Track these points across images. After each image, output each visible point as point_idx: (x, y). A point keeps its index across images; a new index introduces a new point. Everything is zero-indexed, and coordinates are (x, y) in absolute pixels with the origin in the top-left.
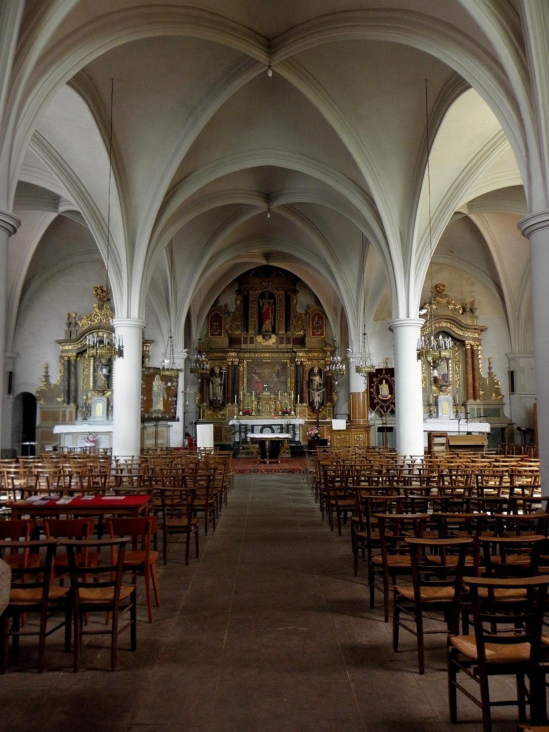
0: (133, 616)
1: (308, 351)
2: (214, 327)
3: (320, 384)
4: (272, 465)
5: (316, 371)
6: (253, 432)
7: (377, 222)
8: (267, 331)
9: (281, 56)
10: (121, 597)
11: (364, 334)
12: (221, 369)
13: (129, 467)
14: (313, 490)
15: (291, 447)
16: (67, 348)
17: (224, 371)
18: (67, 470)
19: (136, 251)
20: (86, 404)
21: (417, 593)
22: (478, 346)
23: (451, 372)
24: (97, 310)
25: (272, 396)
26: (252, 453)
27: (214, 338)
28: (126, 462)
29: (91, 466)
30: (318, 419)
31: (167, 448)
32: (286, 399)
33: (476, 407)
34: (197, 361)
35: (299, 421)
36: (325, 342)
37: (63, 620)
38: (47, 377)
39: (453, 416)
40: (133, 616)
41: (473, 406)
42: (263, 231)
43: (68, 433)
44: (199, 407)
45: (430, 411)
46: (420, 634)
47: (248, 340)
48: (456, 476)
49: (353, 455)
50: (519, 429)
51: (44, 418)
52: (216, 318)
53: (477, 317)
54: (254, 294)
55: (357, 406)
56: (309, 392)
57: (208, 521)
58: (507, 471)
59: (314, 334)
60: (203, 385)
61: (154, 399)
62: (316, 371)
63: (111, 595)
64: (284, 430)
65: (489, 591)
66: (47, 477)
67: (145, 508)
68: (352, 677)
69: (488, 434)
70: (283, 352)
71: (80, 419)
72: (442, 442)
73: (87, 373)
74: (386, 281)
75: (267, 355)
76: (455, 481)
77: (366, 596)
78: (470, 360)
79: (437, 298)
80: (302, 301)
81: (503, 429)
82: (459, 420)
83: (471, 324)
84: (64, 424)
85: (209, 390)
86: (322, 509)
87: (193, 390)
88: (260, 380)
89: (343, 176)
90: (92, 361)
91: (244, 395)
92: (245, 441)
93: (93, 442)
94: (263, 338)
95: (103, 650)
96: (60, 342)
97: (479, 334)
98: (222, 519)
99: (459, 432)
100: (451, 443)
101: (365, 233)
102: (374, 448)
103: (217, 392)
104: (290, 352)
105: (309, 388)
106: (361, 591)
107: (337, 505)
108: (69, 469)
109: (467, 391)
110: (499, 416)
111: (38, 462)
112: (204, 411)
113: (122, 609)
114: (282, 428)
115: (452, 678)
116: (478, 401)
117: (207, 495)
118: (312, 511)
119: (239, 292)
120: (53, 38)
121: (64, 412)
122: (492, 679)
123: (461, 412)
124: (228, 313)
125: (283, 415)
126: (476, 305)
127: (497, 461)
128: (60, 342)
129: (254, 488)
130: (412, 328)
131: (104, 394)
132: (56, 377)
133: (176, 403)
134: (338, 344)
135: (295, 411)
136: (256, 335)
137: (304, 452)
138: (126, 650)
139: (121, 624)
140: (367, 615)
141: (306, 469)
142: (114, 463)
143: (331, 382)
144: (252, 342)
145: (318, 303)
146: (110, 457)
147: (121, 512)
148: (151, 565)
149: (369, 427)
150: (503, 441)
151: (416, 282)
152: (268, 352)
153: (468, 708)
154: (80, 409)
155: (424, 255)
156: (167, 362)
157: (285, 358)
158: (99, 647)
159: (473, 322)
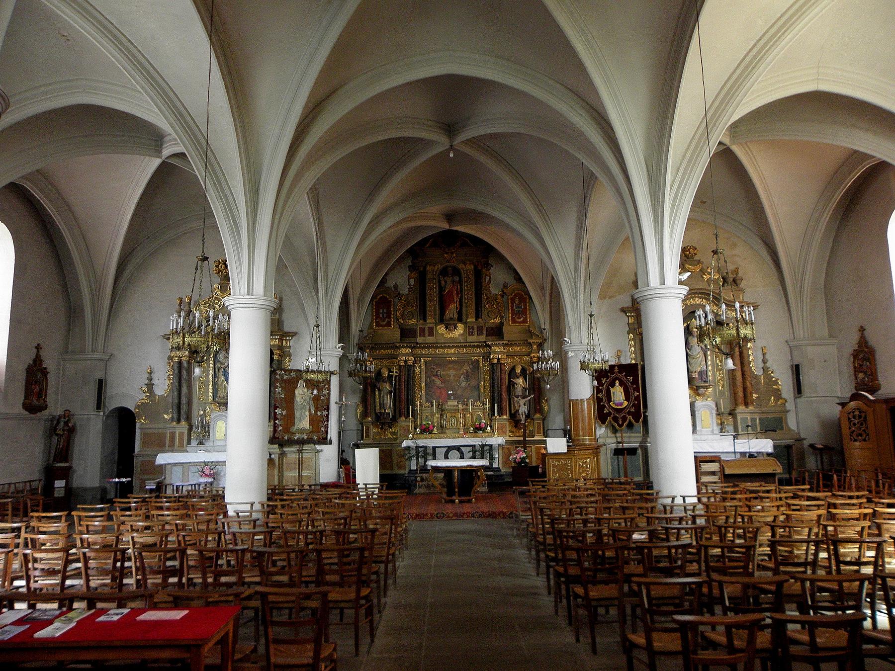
1: (507, 345)
4: (464, 505)
5: (518, 370)
6: (434, 458)
7: (611, 149)
8: (451, 319)
12: (390, 371)
14: (529, 550)
19: (261, 196)
23: (710, 368)
24: (219, 293)
25: (460, 406)
27: (380, 330)
32: (479, 410)
34: (357, 361)
35: (497, 440)
36: (530, 332)
38: (150, 386)
39: (717, 429)
41: (745, 416)
42: (449, 176)
43: (175, 464)
44: (362, 424)
50: (812, 446)
51: (145, 444)
52: (382, 303)
53: (743, 290)
54: (433, 270)
59: (514, 321)
61: (297, 414)
62: (518, 370)
64: (477, 453)
67: (227, 634)
70: (474, 347)
71: (194, 443)
72: (713, 469)
75: (452, 351)
80: (497, 278)
84: (172, 452)
87: (353, 400)
89: (558, 86)
91: (421, 405)
92: (424, 469)
94: (447, 328)
98: (387, 613)
103: (386, 402)
104: (482, 346)
107: (586, 597)
109: (734, 394)
110: (782, 429)
112: (368, 429)
116: (751, 408)
119: (412, 268)
124: (399, 295)
126: (741, 274)
129: (437, 551)
130: (671, 299)
132: (163, 386)
134: (547, 334)
135: (491, 427)
136: (436, 324)
143: (539, 385)
144: (431, 333)
145: (519, 279)
149: (598, 448)
151: (671, 233)
152: (453, 347)
157: (477, 355)
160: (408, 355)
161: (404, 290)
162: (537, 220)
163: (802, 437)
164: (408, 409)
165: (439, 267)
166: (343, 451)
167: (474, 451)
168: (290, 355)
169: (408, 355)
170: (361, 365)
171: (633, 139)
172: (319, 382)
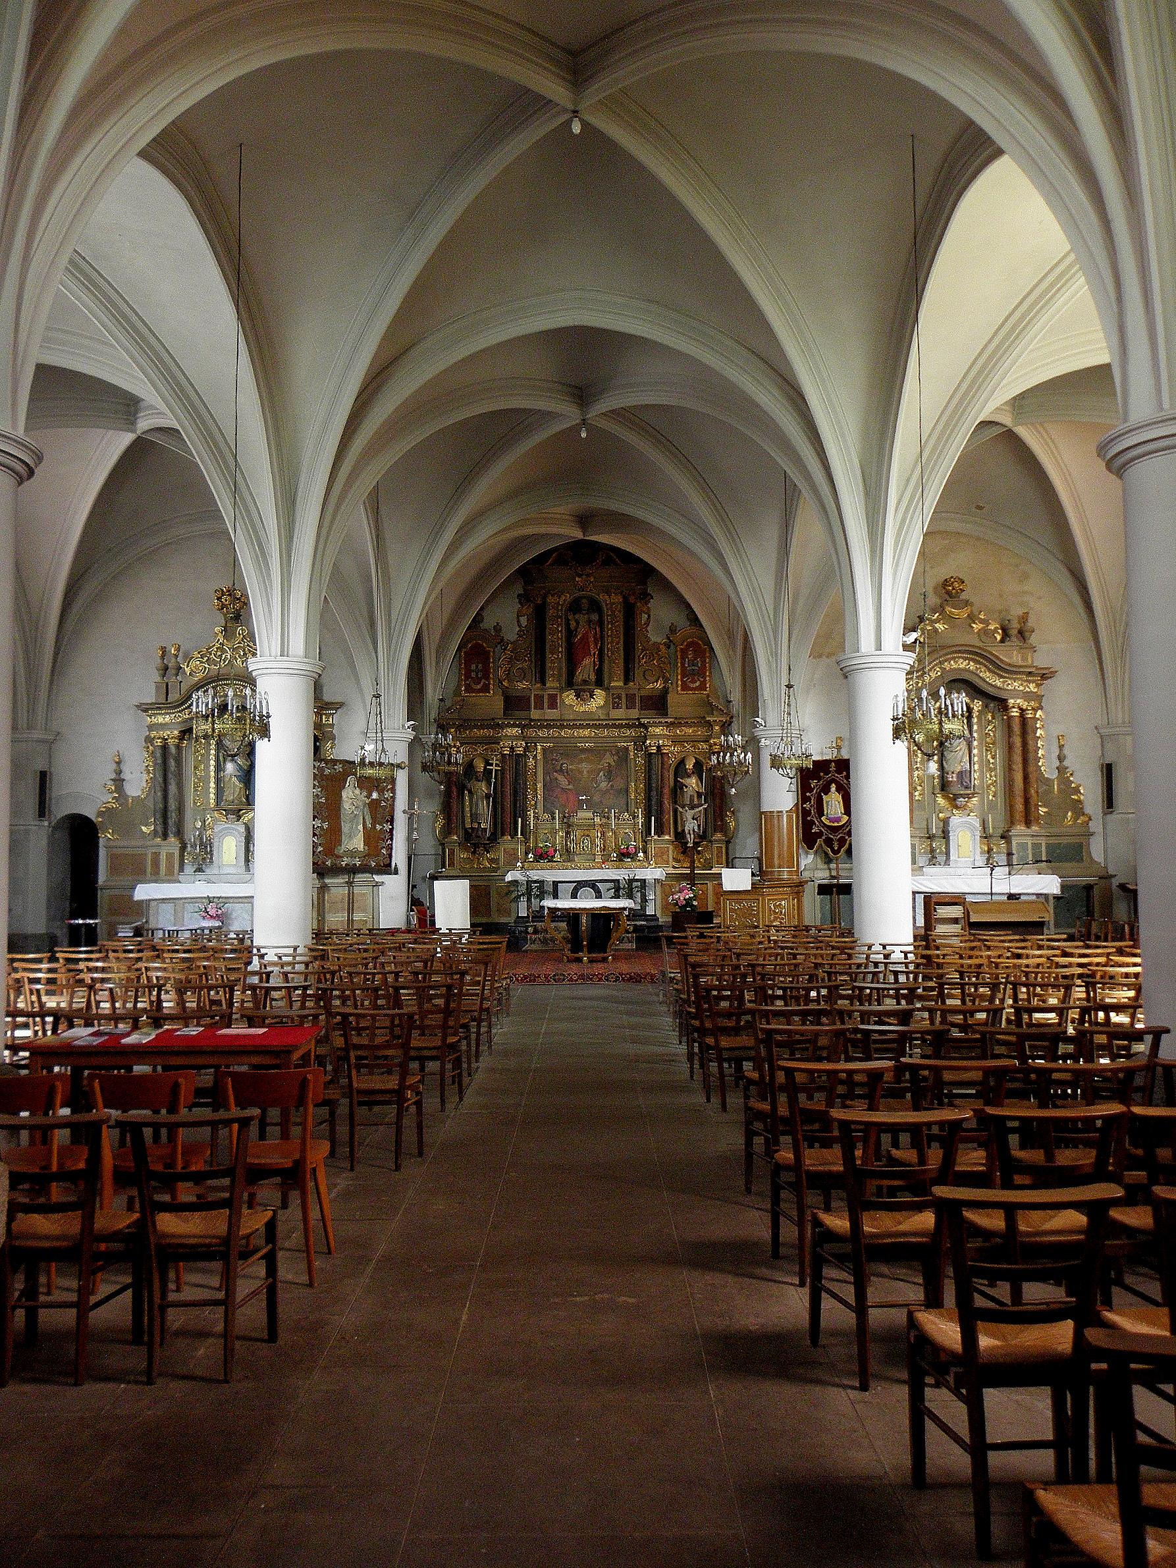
0: (272, 1270)
1: (672, 724)
2: (473, 675)
3: (699, 795)
4: (595, 965)
5: (690, 765)
6: (556, 896)
8: (585, 682)
9: (596, 91)
10: (243, 1232)
11: (789, 686)
12: (488, 763)
13: (287, 969)
14: (675, 1018)
15: (637, 929)
16: (160, 719)
17: (494, 768)
18: (154, 975)
19: (298, 515)
20: (201, 839)
21: (856, 1224)
22: (1035, 710)
25: (597, 820)
26: (553, 940)
27: (473, 698)
28: (280, 958)
29: (204, 967)
30: (692, 868)
31: (370, 930)
32: (627, 825)
33: (1029, 841)
34: (436, 746)
35: (652, 873)
36: (711, 704)
37: (128, 1280)
38: (119, 782)
39: (981, 860)
40: (272, 1270)
42: (579, 464)
45: (932, 851)
46: (861, 1308)
47: (546, 700)
48: (976, 986)
49: (761, 943)
51: (114, 869)
52: (476, 655)
53: (1033, 649)
54: (558, 602)
55: (776, 839)
56: (675, 811)
57: (448, 1081)
58: (1080, 976)
60: (450, 797)
61: (345, 828)
62: (690, 765)
63: (221, 1228)
65: (1006, 1220)
66: (111, 990)
68: (720, 1396)
69: (1057, 898)
70: (620, 726)
71: (189, 869)
73: (203, 775)
74: (834, 575)
75: (586, 732)
76: (974, 998)
77: (764, 1233)
78: (1017, 741)
79: (948, 609)
80: (659, 619)
81: (1089, 888)
82: (992, 870)
83: (1020, 663)
84: (156, 882)
85: (463, 808)
86: (691, 1056)
87: (430, 808)
88: (570, 787)
90: (213, 746)
91: (536, 818)
93: (217, 917)
94: (578, 696)
95: (211, 1340)
96: (145, 708)
97: (1038, 686)
98: (479, 1077)
99: (992, 894)
100: (974, 918)
101: (788, 471)
102: (807, 928)
103: (480, 811)
104: (634, 726)
105: (675, 802)
106: (753, 1224)
107: (717, 1047)
108: (159, 974)
109: (1011, 808)
111: (98, 960)
112: (452, 853)
113: (245, 1255)
114: (618, 889)
115: (917, 1398)
116: (1035, 828)
117: (444, 1027)
118: (670, 1060)
119: (524, 598)
120: (104, 59)
121: (156, 856)
122: (992, 1397)
123: (999, 853)
125: (621, 860)
126: (1030, 624)
127: (1065, 954)
128: (145, 708)
131: (239, 817)
132: (138, 783)
133: (392, 835)
135: (645, 852)
136: (562, 690)
137: (658, 939)
138: (257, 1340)
139: (243, 1288)
140: (764, 1271)
141: (663, 973)
142: (256, 960)
143: (723, 787)
144: (553, 705)
145: (694, 620)
146: (249, 950)
147: (256, 1060)
148: (314, 1170)
149: (801, 884)
150: (1090, 913)
152: (588, 726)
153: (948, 1457)
154: (189, 849)
155: (912, 518)
156: (370, 747)
157: (624, 739)
158: (203, 1334)
159: (1024, 659)
160: (517, 738)
161: (511, 634)
162: (716, 531)
163: (1111, 872)
164: (516, 823)
165: (567, 597)
166: (414, 887)
167: (617, 889)
168: (333, 738)
169: (517, 738)
170: (442, 754)
171: (843, 436)
172: (378, 780)
